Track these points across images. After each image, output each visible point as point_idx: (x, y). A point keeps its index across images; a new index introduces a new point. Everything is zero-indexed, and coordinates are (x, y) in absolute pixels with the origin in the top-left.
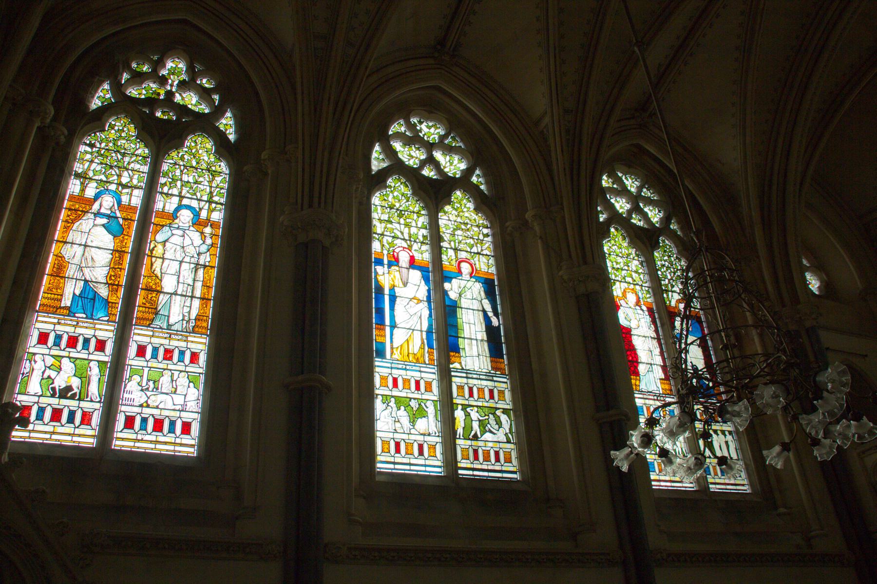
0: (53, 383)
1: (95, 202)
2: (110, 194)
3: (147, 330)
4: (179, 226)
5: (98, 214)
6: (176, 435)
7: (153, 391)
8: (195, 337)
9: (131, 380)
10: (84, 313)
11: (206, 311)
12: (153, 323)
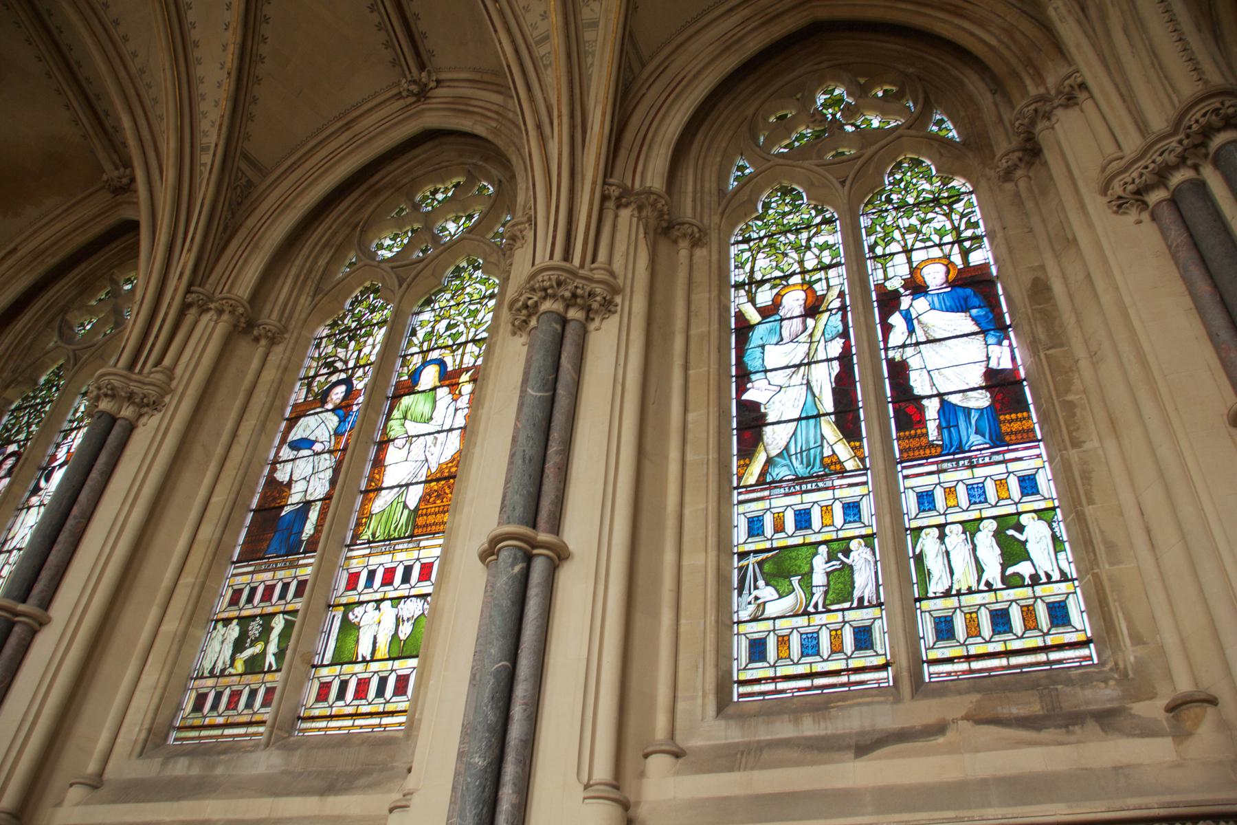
6: (846, 654)
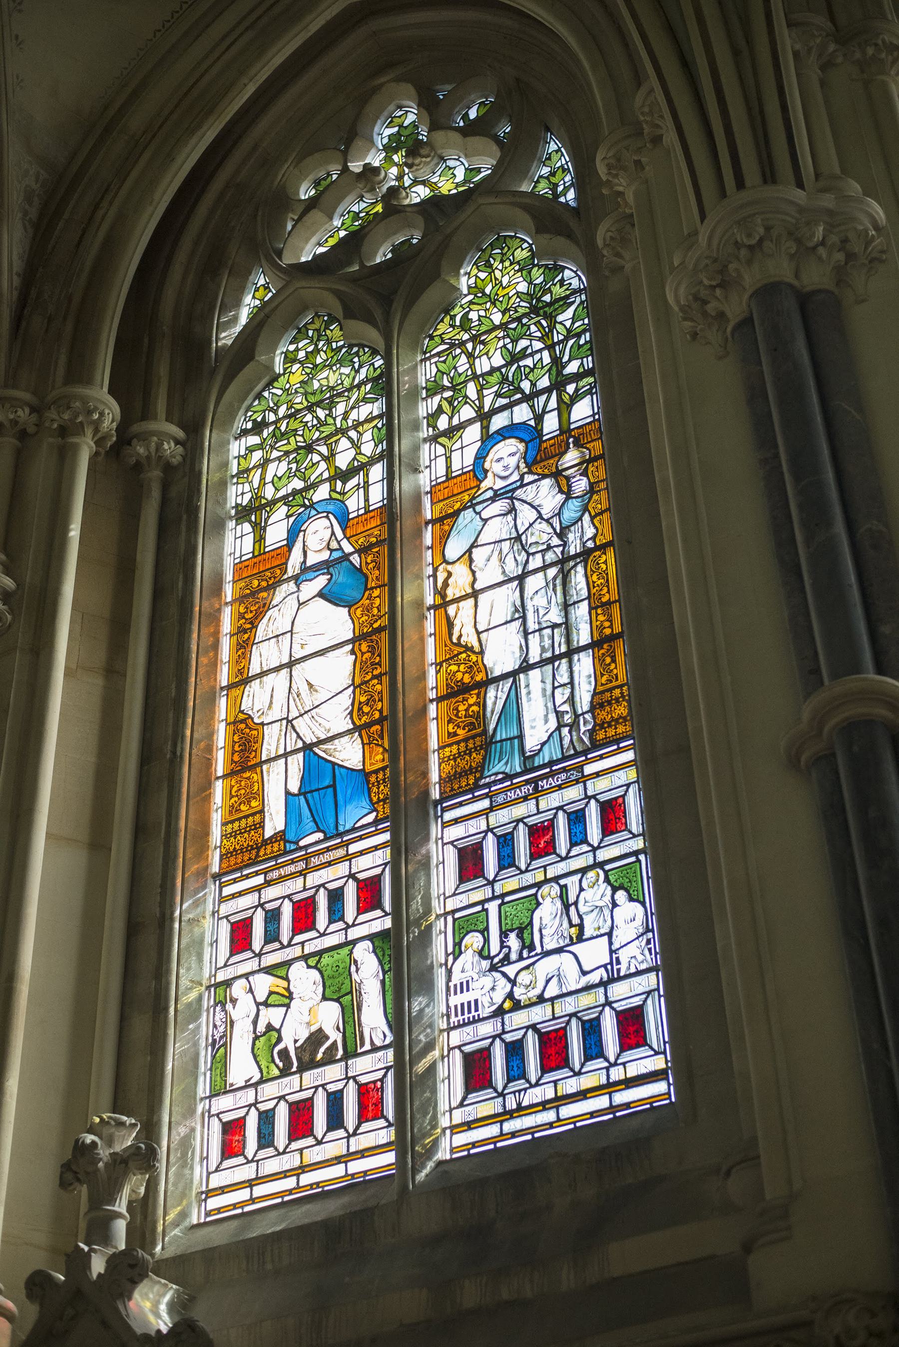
0: (279, 1040)
1: (290, 551)
2: (319, 513)
3: (475, 799)
4: (496, 491)
5: (307, 571)
7: (521, 958)
8: (601, 757)
9: (461, 953)
10: (319, 830)
11: (615, 671)
12: (486, 773)
